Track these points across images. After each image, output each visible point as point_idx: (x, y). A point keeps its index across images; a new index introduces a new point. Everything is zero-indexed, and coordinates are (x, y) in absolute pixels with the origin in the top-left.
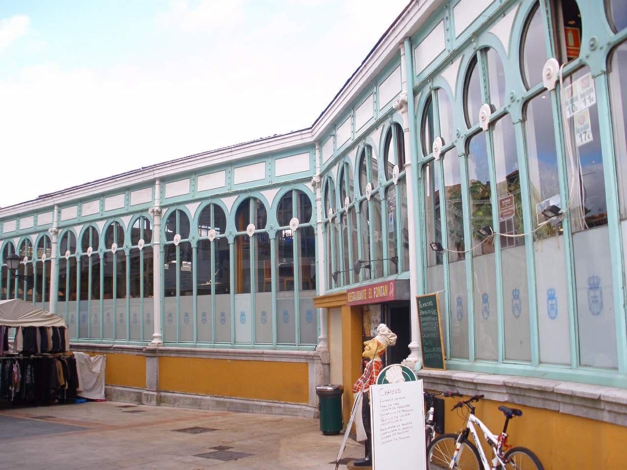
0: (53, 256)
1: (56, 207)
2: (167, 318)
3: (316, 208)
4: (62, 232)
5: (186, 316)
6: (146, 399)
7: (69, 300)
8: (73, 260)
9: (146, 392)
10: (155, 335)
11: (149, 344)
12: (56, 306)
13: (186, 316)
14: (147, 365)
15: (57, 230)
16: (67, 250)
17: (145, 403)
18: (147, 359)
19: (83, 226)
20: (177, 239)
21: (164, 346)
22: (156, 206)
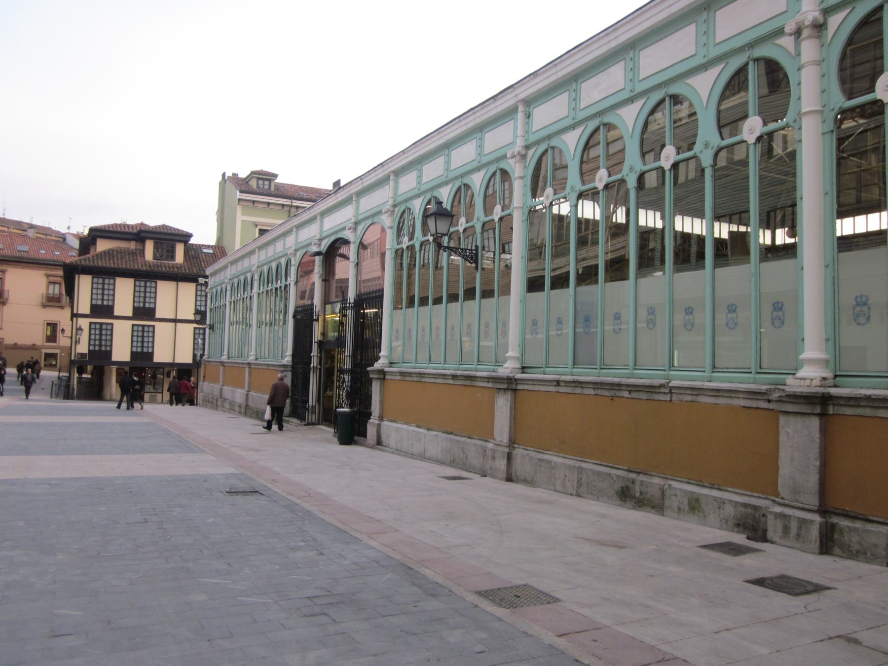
0: (517, 201)
1: (520, 109)
2: (530, 324)
3: (799, 84)
4: (533, 155)
5: (616, 319)
6: (780, 529)
7: (606, 281)
8: (411, 248)
9: (778, 509)
10: (804, 356)
11: (790, 380)
12: (523, 302)
13: (616, 319)
14: (782, 437)
15: (524, 152)
16: (663, 146)
17: (776, 539)
18: (782, 419)
19: (582, 128)
20: (405, 242)
21: (835, 386)
22: (518, 147)
